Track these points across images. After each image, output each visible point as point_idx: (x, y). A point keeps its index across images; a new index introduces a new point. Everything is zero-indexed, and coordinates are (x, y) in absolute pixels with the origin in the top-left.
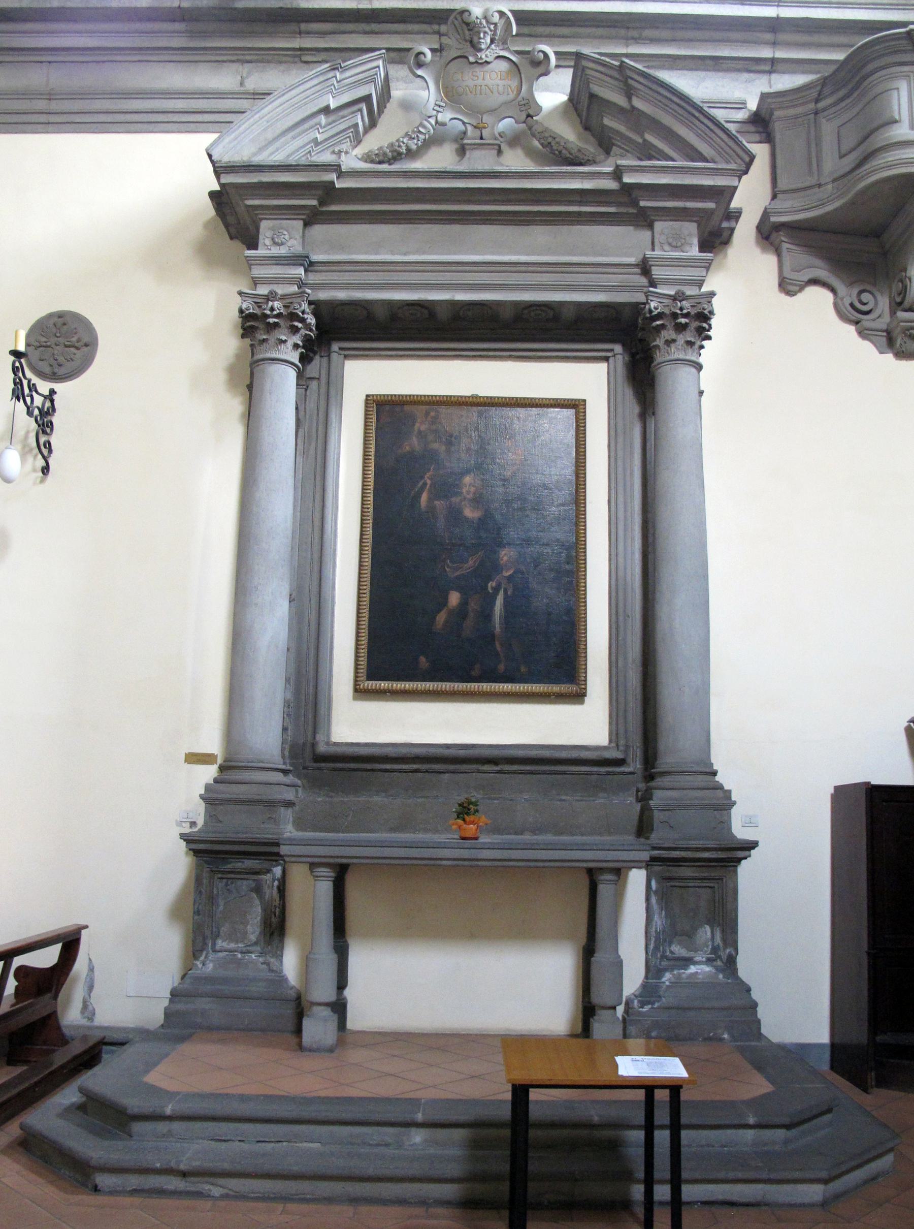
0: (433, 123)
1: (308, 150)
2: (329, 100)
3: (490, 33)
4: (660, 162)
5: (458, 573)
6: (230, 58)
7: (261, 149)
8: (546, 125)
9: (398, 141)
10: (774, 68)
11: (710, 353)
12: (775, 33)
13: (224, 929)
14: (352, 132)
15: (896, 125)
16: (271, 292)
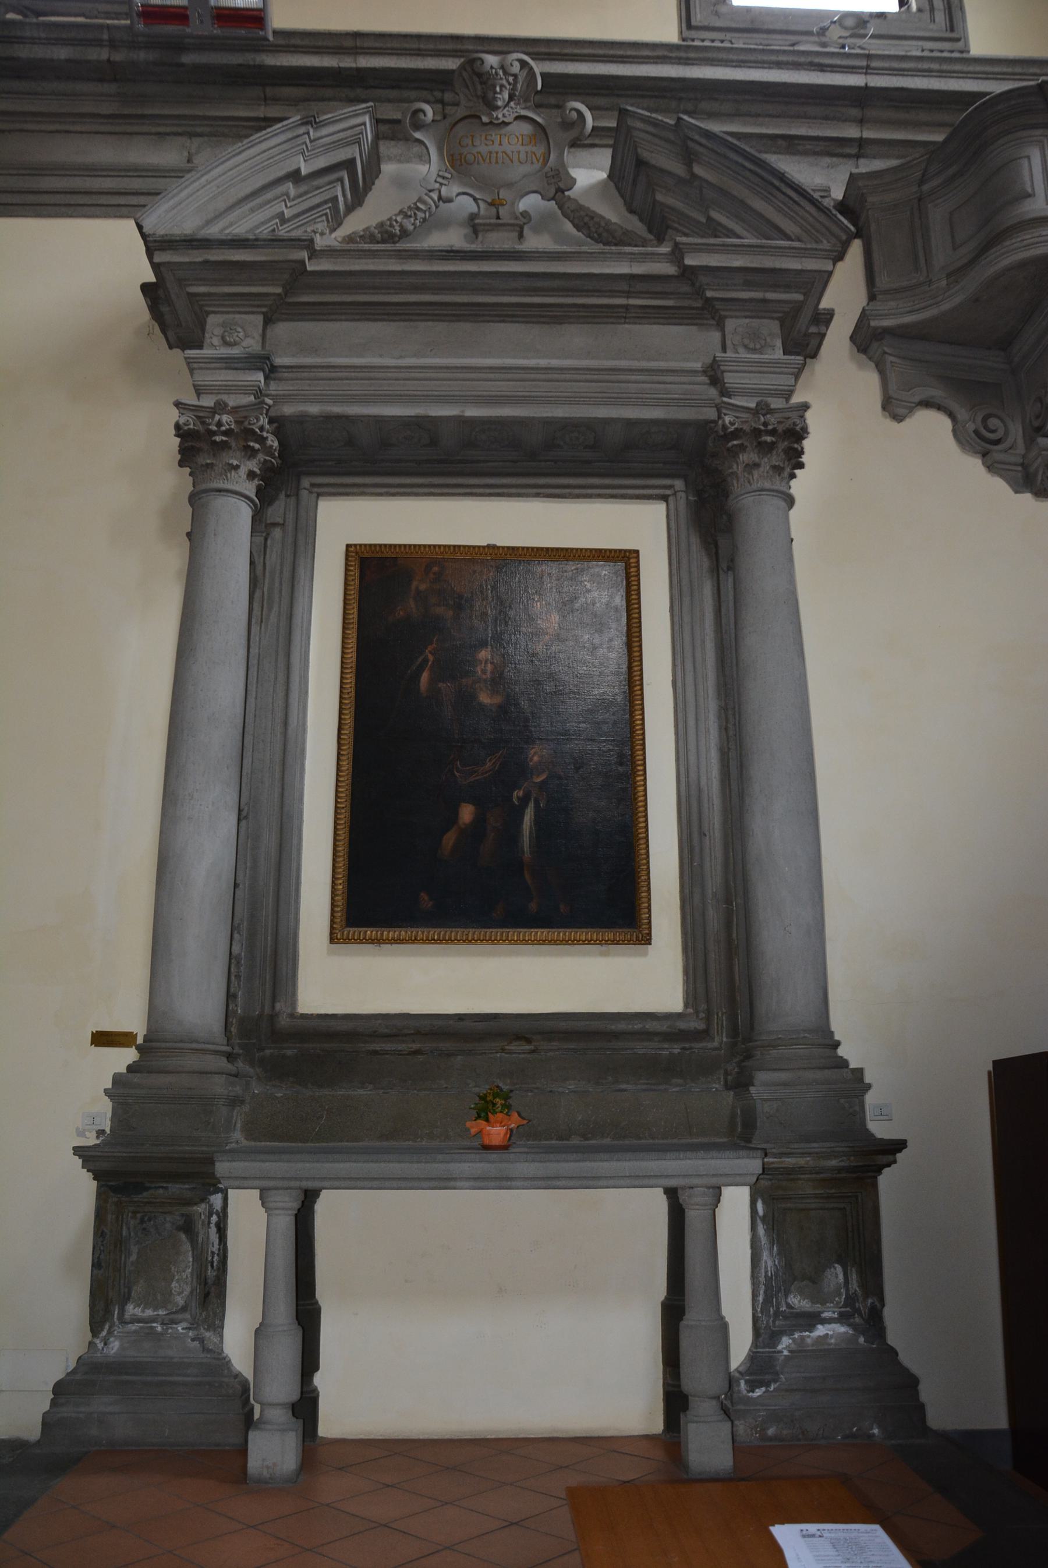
0: (436, 198)
1: (272, 228)
2: (299, 162)
3: (508, 87)
4: (729, 240)
5: (472, 779)
6: (175, 129)
7: (208, 222)
8: (581, 202)
9: (390, 219)
10: (862, 151)
11: (800, 485)
12: (863, 108)
13: (138, 1289)
14: (329, 208)
15: (1029, 200)
16: (218, 403)
